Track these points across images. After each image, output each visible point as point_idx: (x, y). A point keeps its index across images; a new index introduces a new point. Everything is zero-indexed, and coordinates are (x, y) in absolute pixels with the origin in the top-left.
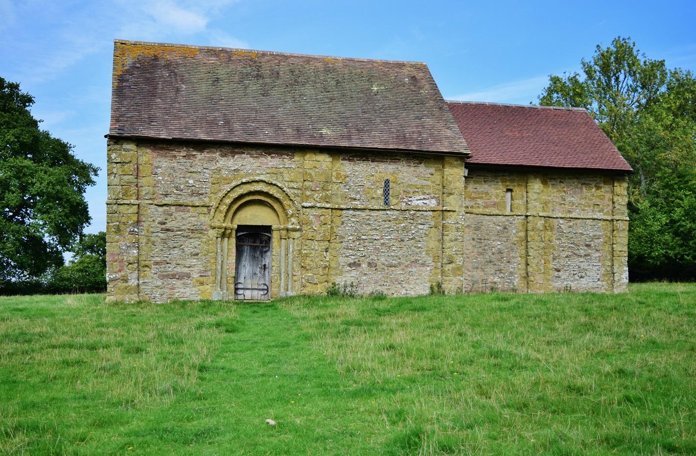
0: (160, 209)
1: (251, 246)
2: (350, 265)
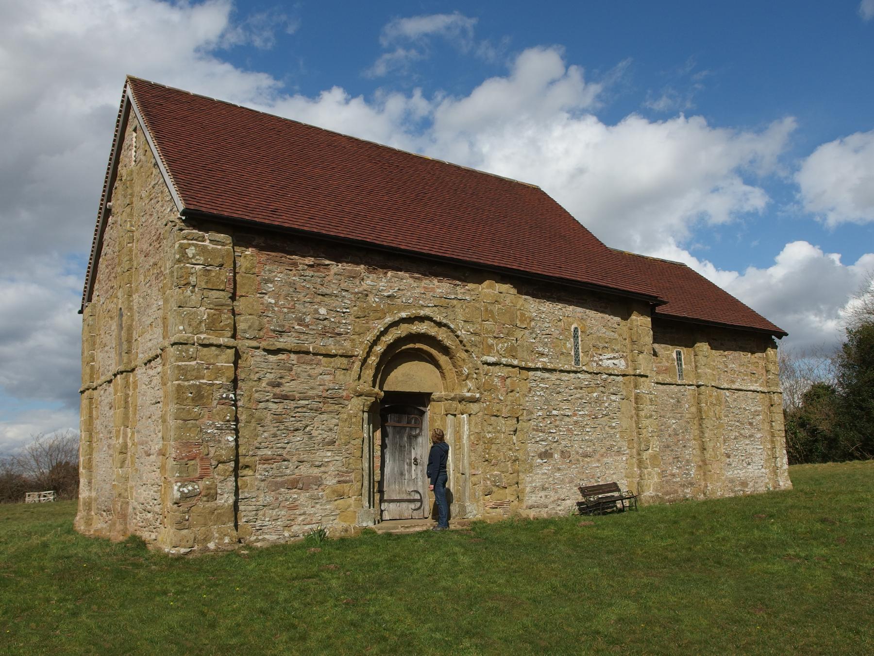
0: (272, 358)
1: (395, 427)
2: (541, 456)
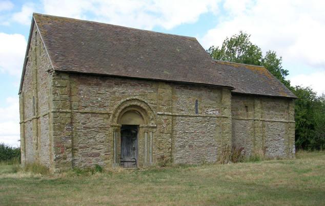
0: (83, 115)
2: (180, 147)
